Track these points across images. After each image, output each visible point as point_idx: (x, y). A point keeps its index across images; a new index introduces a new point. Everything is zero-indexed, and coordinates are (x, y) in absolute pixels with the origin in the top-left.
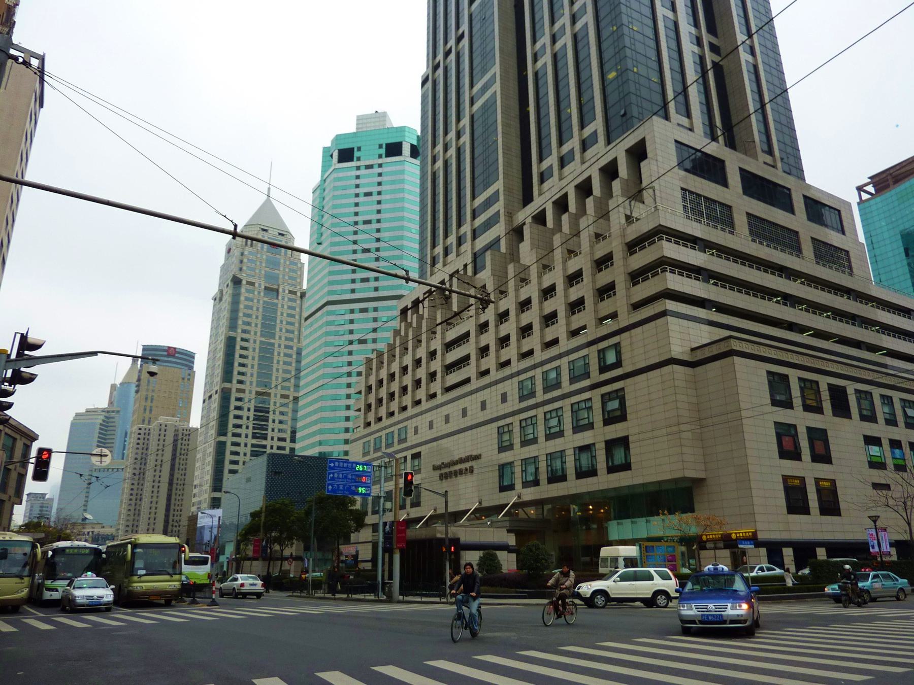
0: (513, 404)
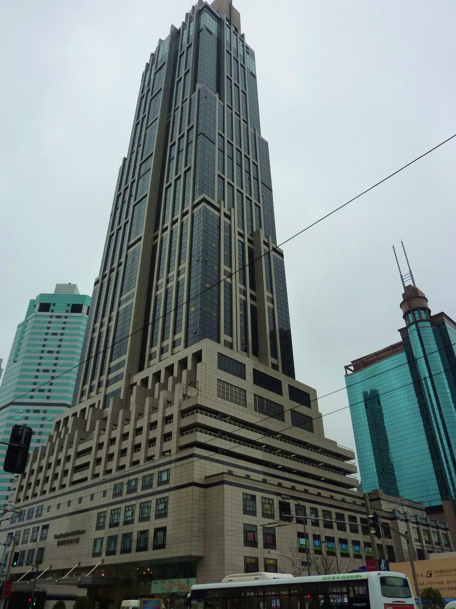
0: (109, 499)
